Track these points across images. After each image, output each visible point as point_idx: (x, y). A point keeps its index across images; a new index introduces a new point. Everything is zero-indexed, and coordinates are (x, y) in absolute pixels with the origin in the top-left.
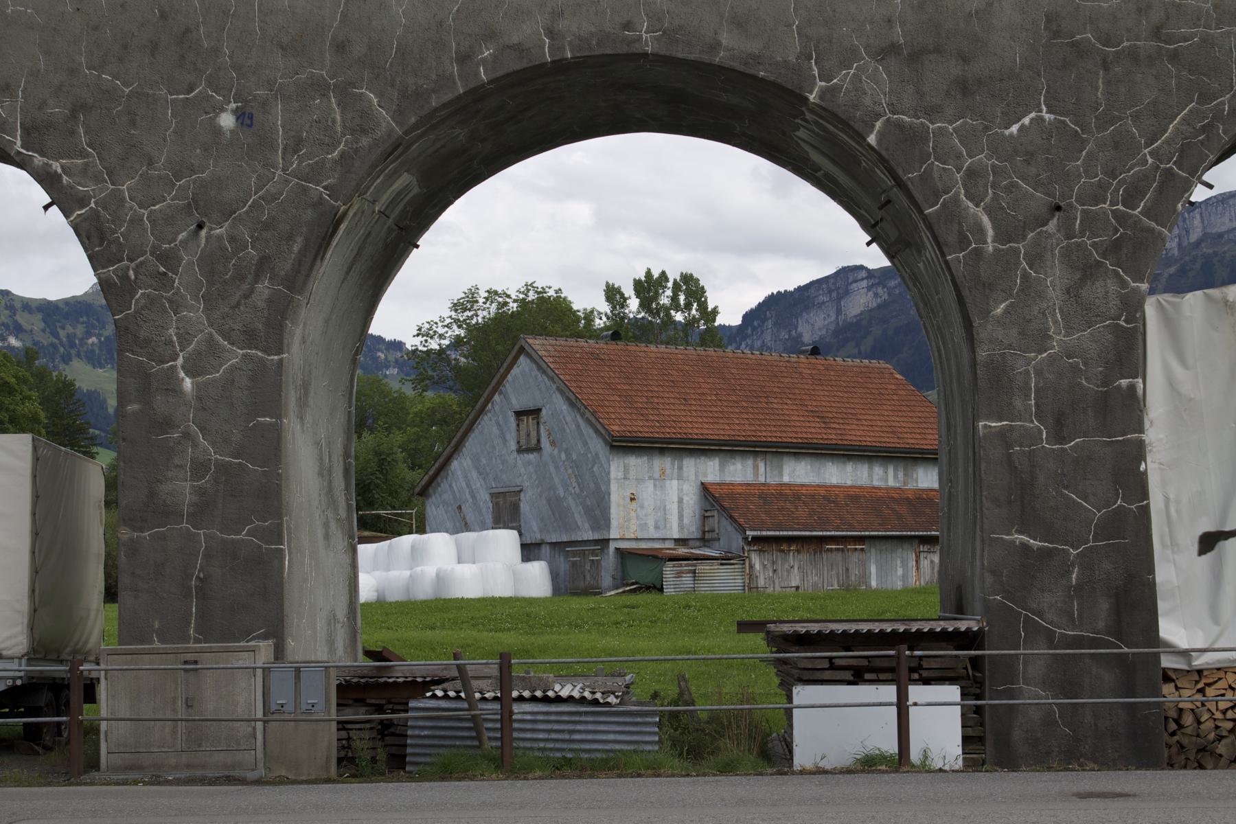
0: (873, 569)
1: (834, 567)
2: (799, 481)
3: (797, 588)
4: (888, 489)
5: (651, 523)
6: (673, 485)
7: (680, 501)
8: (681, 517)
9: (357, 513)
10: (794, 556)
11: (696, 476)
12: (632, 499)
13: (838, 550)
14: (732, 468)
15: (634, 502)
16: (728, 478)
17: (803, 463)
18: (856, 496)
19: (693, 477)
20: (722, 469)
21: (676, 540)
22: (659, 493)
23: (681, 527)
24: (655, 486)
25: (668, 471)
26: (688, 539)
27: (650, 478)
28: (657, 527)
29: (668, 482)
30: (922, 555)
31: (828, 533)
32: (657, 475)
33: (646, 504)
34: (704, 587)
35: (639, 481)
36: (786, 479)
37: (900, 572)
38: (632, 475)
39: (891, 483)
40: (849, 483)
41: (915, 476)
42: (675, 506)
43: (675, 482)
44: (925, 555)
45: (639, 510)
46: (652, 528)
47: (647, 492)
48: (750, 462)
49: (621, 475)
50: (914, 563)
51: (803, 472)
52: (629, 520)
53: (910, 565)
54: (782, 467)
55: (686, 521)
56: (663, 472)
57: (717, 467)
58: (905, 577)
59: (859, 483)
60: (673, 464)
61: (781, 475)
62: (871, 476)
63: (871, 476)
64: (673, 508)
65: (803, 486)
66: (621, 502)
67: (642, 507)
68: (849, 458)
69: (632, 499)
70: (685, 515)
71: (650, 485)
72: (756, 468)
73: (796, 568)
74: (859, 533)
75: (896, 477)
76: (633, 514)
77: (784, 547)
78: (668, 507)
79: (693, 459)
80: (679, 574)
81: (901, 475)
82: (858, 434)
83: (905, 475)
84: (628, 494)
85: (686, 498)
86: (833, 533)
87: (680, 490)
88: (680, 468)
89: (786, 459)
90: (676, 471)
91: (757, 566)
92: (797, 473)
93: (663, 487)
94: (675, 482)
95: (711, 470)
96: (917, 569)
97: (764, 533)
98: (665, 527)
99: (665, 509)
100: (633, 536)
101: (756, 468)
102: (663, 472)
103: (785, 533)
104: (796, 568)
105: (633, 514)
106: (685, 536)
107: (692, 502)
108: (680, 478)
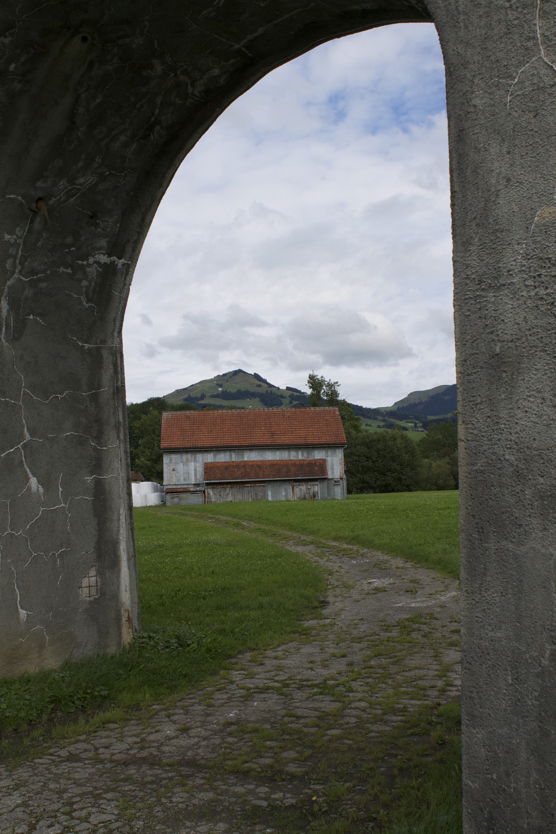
0: (270, 493)
1: (250, 493)
2: (252, 459)
3: (231, 501)
4: (300, 460)
5: (182, 478)
6: (192, 465)
7: (195, 470)
8: (196, 476)
9: (454, 463)
10: (229, 489)
11: (203, 460)
12: (173, 470)
13: (251, 486)
14: (219, 456)
15: (174, 472)
16: (217, 460)
17: (254, 453)
18: (273, 465)
19: (201, 461)
20: (214, 457)
21: (194, 484)
22: (185, 467)
23: (196, 479)
24: (184, 465)
25: (190, 459)
26: (200, 484)
27: (181, 462)
28: (185, 480)
29: (190, 463)
30: (295, 487)
31: (244, 480)
32: (184, 461)
33: (180, 472)
34: (183, 503)
35: (176, 463)
36: (246, 459)
37: (284, 494)
38: (173, 461)
39: (300, 457)
40: (278, 459)
41: (313, 454)
42: (193, 472)
43: (193, 463)
44: (297, 486)
45: (176, 474)
46: (182, 480)
47: (181, 468)
48: (228, 454)
49: (168, 462)
50: (291, 490)
51: (254, 456)
52: (172, 478)
53: (289, 491)
54: (243, 455)
55: (198, 477)
56: (187, 460)
57: (212, 456)
58: (286, 496)
59: (283, 459)
60: (192, 456)
61: (244, 458)
62: (289, 456)
63: (289, 456)
64: (192, 472)
65: (218, 463)
66: (169, 471)
67: (178, 473)
68: (278, 449)
69: (173, 470)
70: (197, 474)
71: (181, 465)
72: (231, 456)
73: (230, 494)
74: (210, 481)
75: (303, 455)
76: (174, 476)
77: (225, 486)
78: (190, 472)
79: (201, 454)
80: (173, 498)
81: (305, 454)
82: (286, 440)
83: (308, 454)
84: (171, 468)
85: (198, 469)
86: (246, 480)
87: (195, 466)
88: (195, 458)
89: (245, 451)
90: (193, 459)
91: (211, 494)
92: (251, 457)
93: (187, 465)
94: (193, 463)
95: (210, 458)
96: (293, 492)
97: (212, 481)
98: (189, 480)
99: (188, 473)
100: (173, 484)
101: (231, 456)
102: (187, 460)
103: (225, 481)
104: (230, 494)
105: (174, 476)
106: (198, 483)
107: (201, 470)
108: (195, 461)
